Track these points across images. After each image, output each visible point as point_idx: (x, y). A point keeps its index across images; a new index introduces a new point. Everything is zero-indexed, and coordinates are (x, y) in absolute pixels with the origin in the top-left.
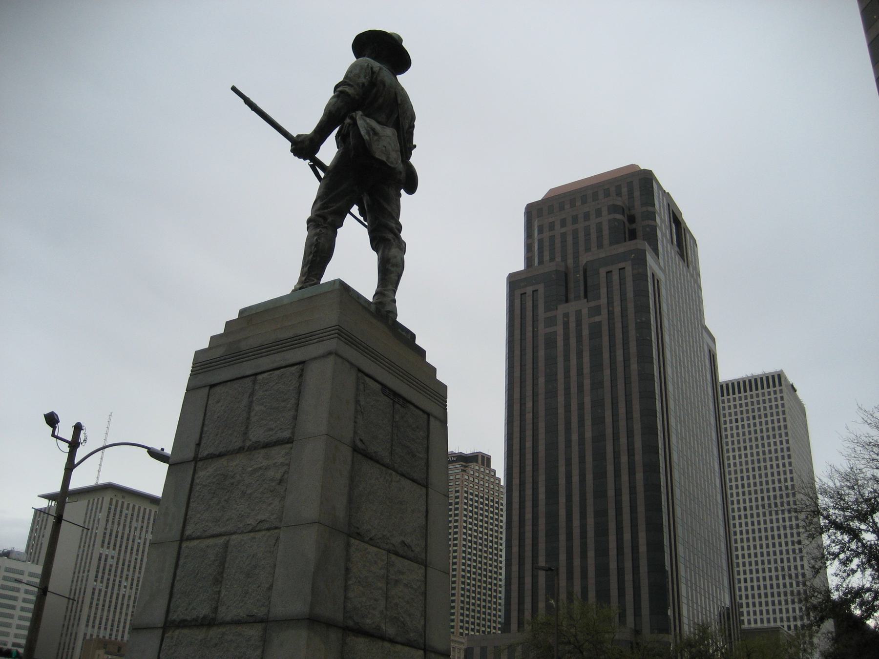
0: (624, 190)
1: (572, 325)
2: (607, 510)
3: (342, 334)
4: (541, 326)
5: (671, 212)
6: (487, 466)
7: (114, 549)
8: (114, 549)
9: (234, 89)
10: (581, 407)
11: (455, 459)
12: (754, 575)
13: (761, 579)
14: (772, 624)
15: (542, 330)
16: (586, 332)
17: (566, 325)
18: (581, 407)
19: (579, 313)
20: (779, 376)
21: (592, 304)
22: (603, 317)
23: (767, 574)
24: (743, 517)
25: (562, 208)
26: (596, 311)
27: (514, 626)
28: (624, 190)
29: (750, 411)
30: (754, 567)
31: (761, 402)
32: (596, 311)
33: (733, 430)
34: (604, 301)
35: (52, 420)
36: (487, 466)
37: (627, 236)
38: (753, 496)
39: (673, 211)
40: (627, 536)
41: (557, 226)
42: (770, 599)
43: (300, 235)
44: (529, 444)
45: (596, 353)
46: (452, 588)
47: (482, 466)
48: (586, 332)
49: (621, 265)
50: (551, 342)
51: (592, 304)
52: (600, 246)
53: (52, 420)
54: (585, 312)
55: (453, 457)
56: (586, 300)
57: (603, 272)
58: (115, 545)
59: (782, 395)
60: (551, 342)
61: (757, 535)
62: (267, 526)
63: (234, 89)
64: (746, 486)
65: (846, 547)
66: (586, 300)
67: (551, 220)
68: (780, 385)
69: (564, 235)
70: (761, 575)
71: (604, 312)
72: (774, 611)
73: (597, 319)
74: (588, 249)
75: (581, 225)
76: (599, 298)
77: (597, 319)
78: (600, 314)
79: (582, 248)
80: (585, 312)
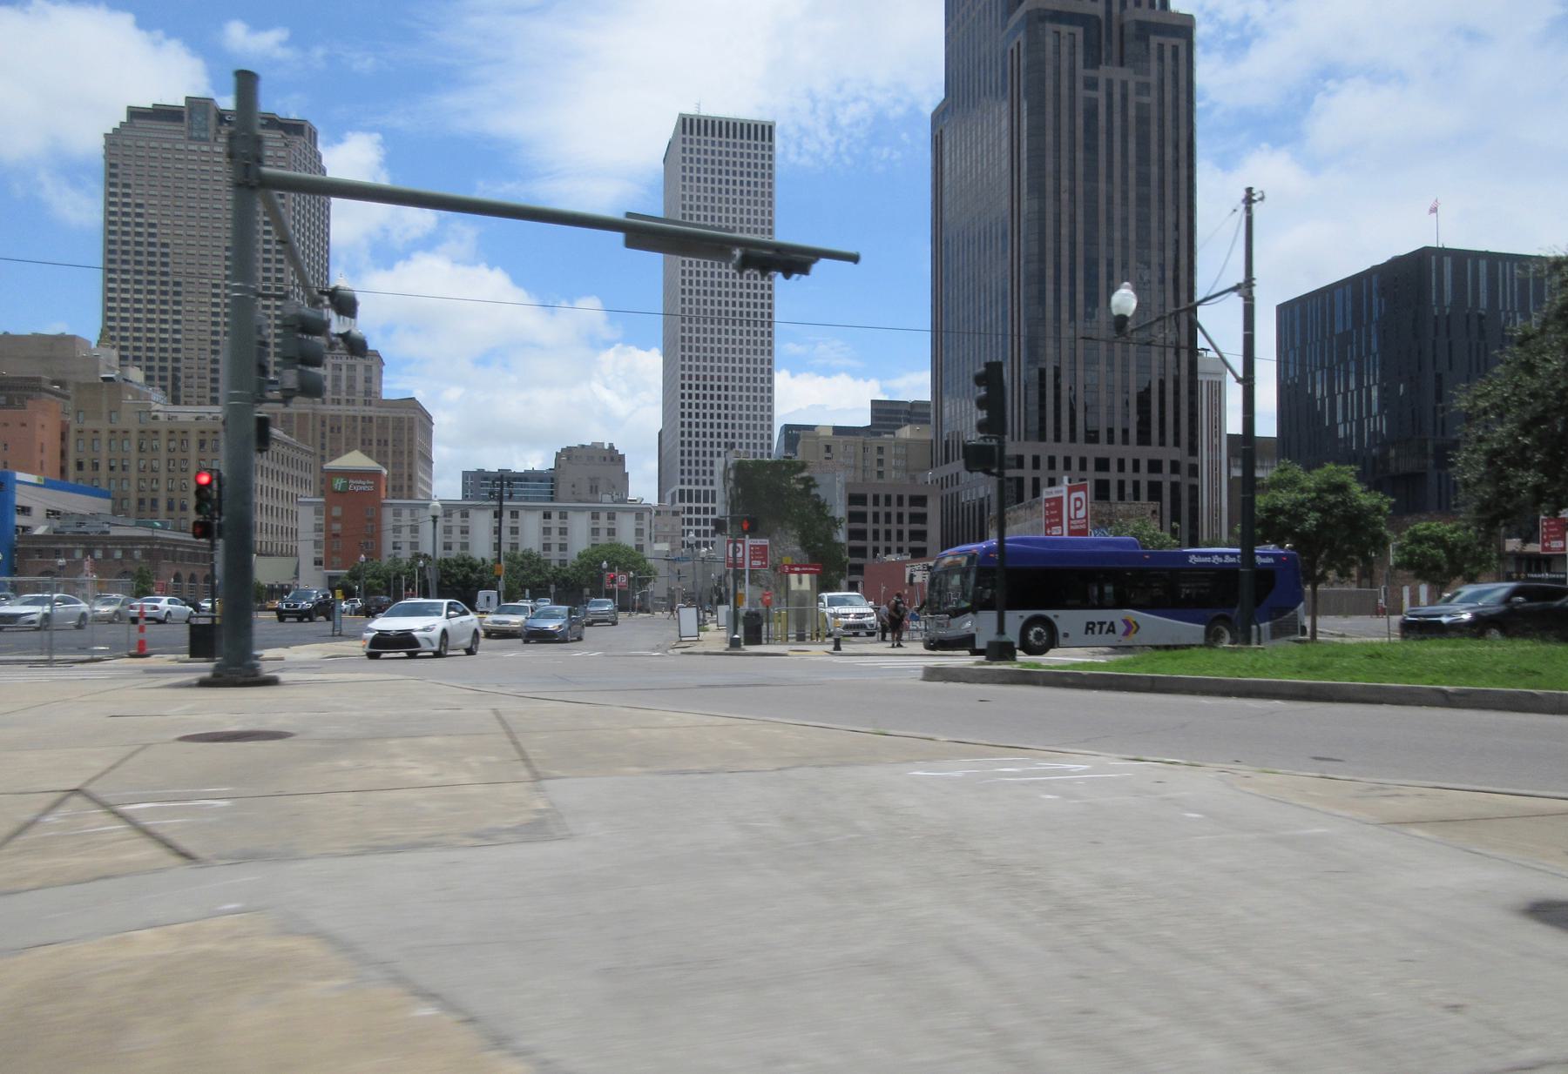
1: (1117, 97)
7: (1177, 443)
8: (1177, 443)
9: (854, 258)
12: (694, 458)
16: (1132, 112)
17: (1110, 95)
18: (1110, 177)
26: (1143, 88)
34: (1153, 79)
40: (1065, 231)
43: (1255, 275)
44: (1065, 231)
48: (1132, 112)
58: (1177, 434)
59: (683, 410)
63: (854, 258)
72: (690, 453)
78: (1149, 94)
80: (1132, 86)
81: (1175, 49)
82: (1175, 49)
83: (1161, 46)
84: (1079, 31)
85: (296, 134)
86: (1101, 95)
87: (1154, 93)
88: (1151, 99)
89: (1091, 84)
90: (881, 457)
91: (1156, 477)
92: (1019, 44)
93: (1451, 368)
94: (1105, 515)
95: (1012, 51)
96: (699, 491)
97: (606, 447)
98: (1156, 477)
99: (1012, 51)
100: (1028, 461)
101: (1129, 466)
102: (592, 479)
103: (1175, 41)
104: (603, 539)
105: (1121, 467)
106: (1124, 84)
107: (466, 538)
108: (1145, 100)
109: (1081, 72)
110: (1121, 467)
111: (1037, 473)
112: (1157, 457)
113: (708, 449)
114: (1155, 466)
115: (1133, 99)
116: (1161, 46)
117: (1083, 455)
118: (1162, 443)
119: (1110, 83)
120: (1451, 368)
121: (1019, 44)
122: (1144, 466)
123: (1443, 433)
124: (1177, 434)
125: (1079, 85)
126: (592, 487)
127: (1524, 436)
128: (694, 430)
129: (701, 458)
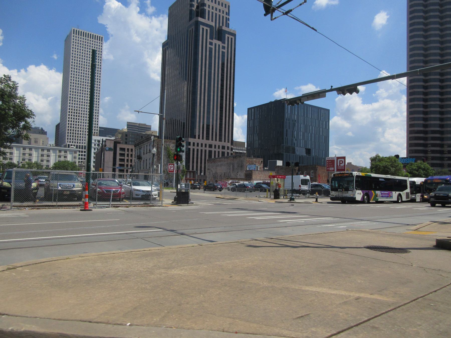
7: (228, 142)
16: (221, 53)
48: (221, 53)
58: (228, 139)
80: (221, 46)
81: (232, 39)
82: (232, 39)
83: (228, 37)
84: (209, 29)
85: (424, 105)
86: (213, 47)
87: (226, 49)
88: (225, 51)
89: (211, 44)
90: (126, 137)
91: (223, 150)
92: (192, 29)
93: (289, 129)
94: (251, 161)
95: (190, 31)
96: (80, 145)
97: (40, 129)
98: (223, 150)
99: (190, 31)
100: (192, 144)
101: (196, 144)
102: (35, 139)
103: (232, 37)
104: (62, 159)
105: (194, 145)
106: (219, 45)
107: (59, 159)
108: (224, 50)
109: (209, 40)
110: (194, 145)
111: (194, 147)
112: (224, 145)
113: (77, 132)
114: (210, 146)
115: (221, 50)
116: (228, 37)
117: (194, 142)
118: (225, 141)
119: (215, 44)
120: (289, 129)
121: (192, 29)
122: (208, 146)
123: (287, 144)
124: (228, 139)
125: (208, 43)
126: (35, 141)
127: (24, 125)
128: (72, 126)
129: (74, 135)
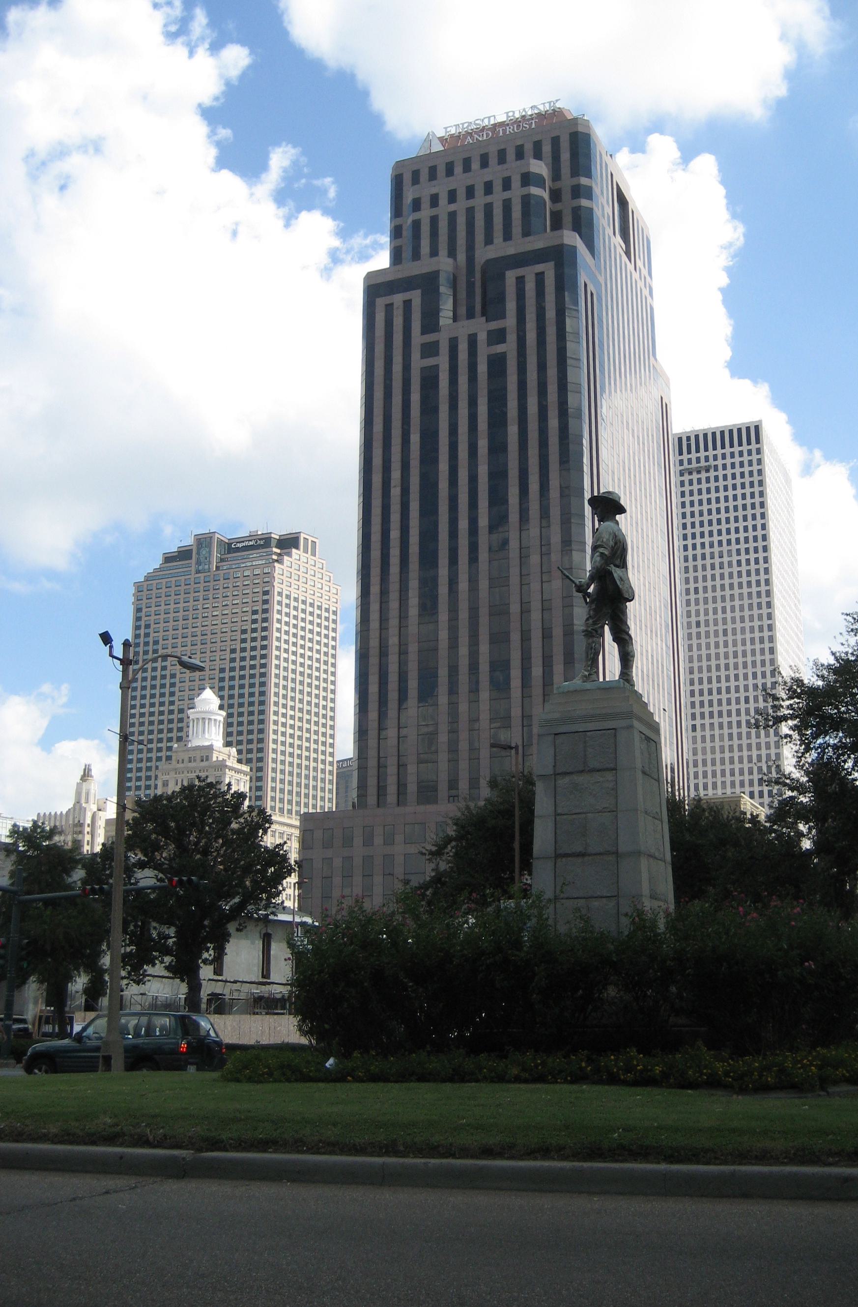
0: (547, 149)
2: (507, 634)
3: (681, 787)
4: (416, 355)
5: (615, 187)
6: (312, 555)
10: (473, 479)
11: (262, 543)
12: (707, 721)
13: (716, 726)
14: (729, 791)
15: (417, 362)
16: (482, 368)
19: (472, 341)
20: (757, 428)
21: (494, 325)
22: (509, 347)
23: (725, 719)
24: (715, 692)
25: (450, 171)
26: (498, 336)
27: (372, 799)
28: (547, 149)
29: (715, 522)
30: (706, 710)
31: (733, 531)
32: (498, 336)
33: (718, 637)
34: (510, 321)
35: (106, 638)
36: (312, 555)
37: (574, 308)
38: (711, 606)
39: (617, 185)
41: (443, 200)
42: (727, 755)
45: (497, 398)
46: (131, 714)
47: (313, 558)
48: (482, 368)
49: (539, 268)
50: (430, 380)
51: (494, 325)
52: (507, 236)
53: (106, 638)
54: (482, 337)
55: (260, 539)
56: (484, 318)
57: (511, 276)
60: (430, 380)
61: (713, 663)
62: (609, 810)
64: (734, 725)
65: (775, 831)
66: (484, 318)
67: (434, 191)
68: (758, 441)
69: (452, 216)
70: (716, 720)
71: (512, 338)
73: (500, 348)
74: (489, 240)
75: (480, 201)
76: (502, 315)
77: (500, 348)
79: (479, 237)
80: (482, 337)
